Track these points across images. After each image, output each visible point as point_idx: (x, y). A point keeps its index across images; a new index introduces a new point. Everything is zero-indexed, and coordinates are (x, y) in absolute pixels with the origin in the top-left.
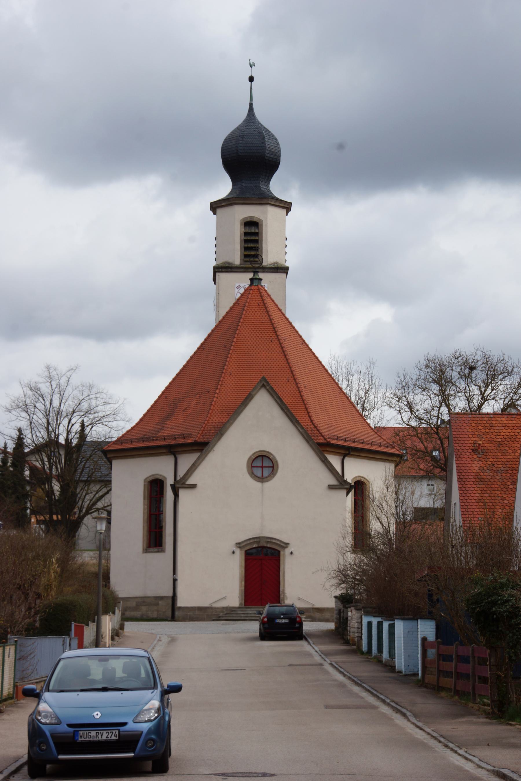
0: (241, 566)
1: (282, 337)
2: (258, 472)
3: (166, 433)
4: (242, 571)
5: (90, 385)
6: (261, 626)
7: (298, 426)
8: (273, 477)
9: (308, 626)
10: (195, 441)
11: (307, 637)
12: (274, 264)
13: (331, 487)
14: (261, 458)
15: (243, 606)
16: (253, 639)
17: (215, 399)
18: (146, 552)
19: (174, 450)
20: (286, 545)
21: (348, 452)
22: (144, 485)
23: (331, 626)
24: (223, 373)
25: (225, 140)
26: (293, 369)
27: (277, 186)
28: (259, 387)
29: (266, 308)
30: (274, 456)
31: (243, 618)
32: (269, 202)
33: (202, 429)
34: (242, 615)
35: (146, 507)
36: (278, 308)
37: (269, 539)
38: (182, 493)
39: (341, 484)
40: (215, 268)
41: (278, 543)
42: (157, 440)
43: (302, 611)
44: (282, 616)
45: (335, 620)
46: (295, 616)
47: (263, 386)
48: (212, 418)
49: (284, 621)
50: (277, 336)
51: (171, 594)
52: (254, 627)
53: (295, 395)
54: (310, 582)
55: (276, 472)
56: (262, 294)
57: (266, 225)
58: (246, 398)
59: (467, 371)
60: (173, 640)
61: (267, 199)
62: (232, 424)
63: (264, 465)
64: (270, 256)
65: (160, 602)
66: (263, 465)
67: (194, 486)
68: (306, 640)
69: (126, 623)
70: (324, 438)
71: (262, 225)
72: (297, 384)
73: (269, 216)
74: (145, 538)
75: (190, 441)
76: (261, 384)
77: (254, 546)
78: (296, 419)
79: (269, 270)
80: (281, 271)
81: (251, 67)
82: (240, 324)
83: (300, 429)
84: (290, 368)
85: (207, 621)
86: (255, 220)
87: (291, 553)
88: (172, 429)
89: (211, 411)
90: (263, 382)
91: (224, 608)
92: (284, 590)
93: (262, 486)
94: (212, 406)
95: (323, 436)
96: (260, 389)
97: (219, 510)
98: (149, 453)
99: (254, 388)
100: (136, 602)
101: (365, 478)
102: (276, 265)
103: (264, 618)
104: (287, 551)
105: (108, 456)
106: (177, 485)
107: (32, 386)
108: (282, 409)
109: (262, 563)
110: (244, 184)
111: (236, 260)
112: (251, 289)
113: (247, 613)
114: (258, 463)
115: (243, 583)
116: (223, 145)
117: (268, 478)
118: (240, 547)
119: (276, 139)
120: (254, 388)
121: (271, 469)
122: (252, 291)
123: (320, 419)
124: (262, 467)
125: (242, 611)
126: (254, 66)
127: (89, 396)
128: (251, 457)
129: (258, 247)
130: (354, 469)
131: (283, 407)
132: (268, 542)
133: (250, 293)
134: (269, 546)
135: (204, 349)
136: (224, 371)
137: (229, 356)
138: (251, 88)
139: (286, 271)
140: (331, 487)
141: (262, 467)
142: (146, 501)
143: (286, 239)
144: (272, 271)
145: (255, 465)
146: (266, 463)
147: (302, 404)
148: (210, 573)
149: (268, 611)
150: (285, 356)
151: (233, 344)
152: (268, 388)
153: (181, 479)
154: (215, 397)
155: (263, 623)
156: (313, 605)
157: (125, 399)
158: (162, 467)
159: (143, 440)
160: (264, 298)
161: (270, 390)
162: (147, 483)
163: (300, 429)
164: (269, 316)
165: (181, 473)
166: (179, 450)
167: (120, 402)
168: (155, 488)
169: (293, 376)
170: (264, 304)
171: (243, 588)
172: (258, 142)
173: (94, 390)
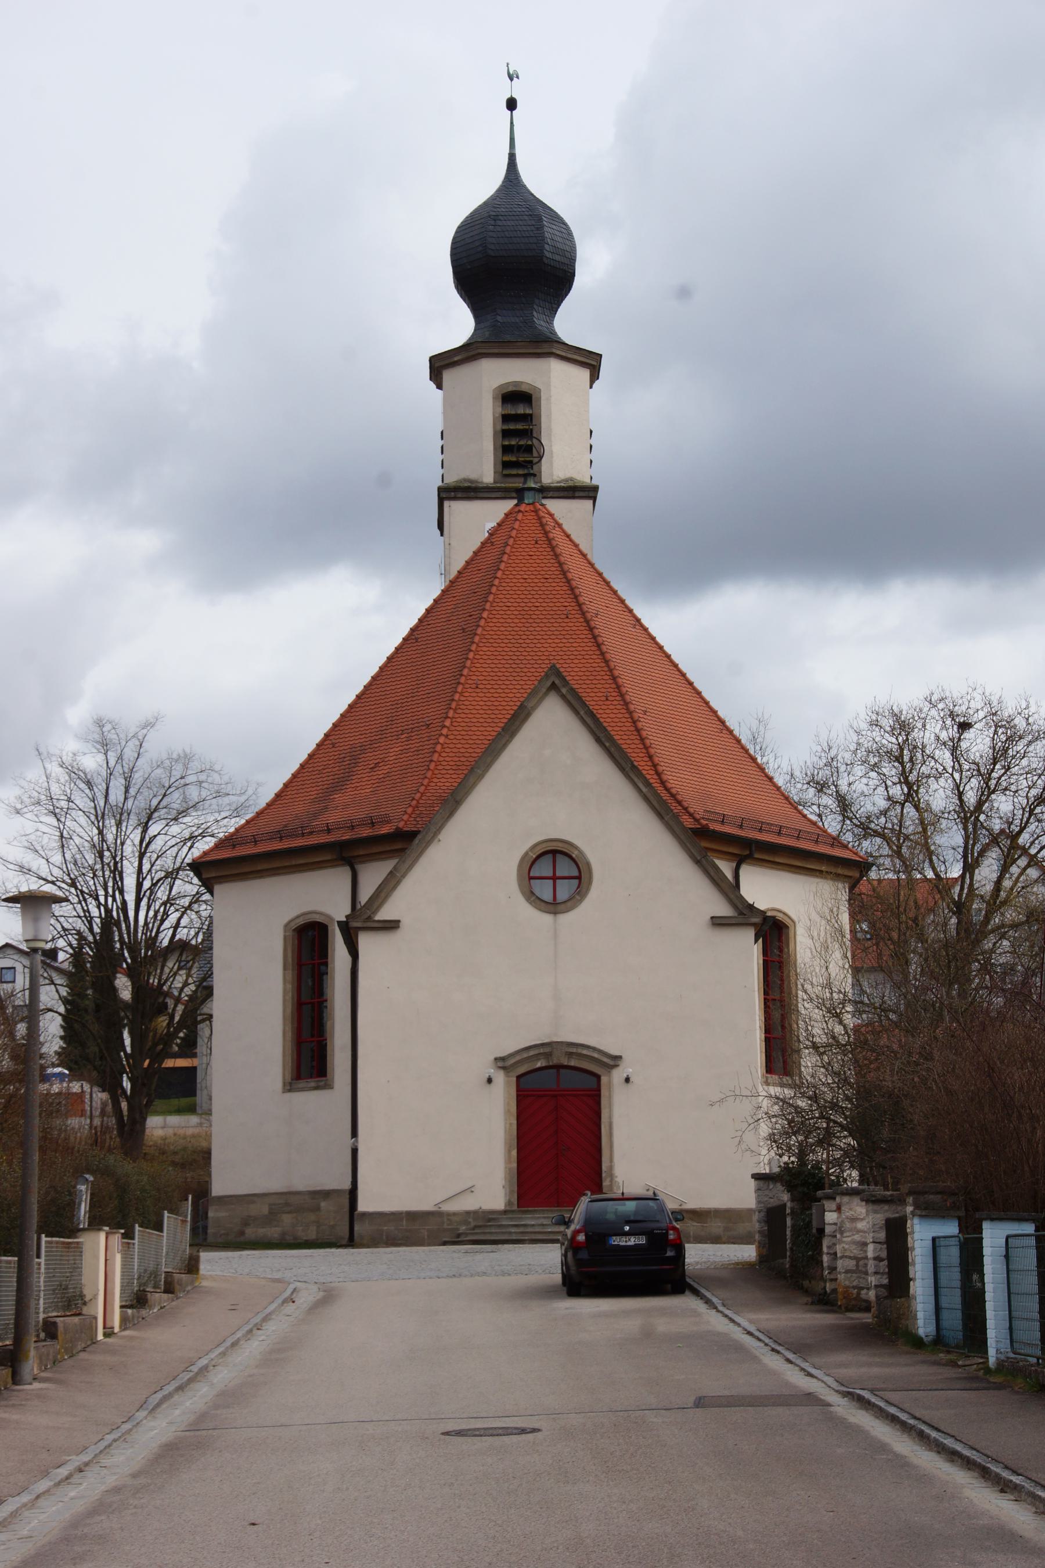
0: (507, 1112)
1: (590, 608)
2: (545, 890)
3: (332, 817)
4: (511, 1124)
5: (186, 756)
6: (570, 1255)
7: (636, 780)
8: (581, 901)
9: (697, 1256)
10: (398, 828)
11: (696, 1286)
12: (566, 480)
13: (718, 922)
14: (550, 856)
15: (515, 1207)
16: (547, 1293)
17: (442, 740)
18: (290, 1091)
19: (346, 853)
20: (616, 1060)
21: (747, 852)
22: (285, 938)
23: (748, 1252)
24: (459, 683)
25: (459, 227)
26: (616, 673)
27: (569, 322)
28: (544, 690)
29: (553, 548)
30: (581, 852)
31: (514, 1237)
32: (554, 351)
33: (414, 803)
34: (513, 1230)
35: (289, 986)
36: (580, 551)
37: (573, 1049)
38: (366, 942)
39: (744, 915)
40: (439, 489)
41: (596, 1055)
42: (311, 833)
43: (680, 1215)
44: (627, 1228)
45: (757, 1237)
46: (663, 1225)
47: (553, 687)
48: (435, 780)
49: (632, 1241)
50: (580, 605)
51: (347, 1185)
52: (547, 1261)
53: (624, 729)
54: (696, 1135)
55: (588, 889)
56: (544, 520)
57: (549, 399)
58: (513, 715)
59: (953, 732)
60: (328, 1297)
61: (545, 345)
62: (481, 777)
63: (558, 874)
64: (559, 463)
65: (323, 1204)
66: (556, 873)
67: (392, 926)
68: (696, 1293)
69: (205, 1256)
70: (694, 818)
71: (540, 398)
72: (626, 704)
73: (555, 382)
74: (289, 1059)
75: (385, 830)
76: (549, 684)
77: (539, 1065)
78: (632, 762)
79: (556, 494)
80: (581, 494)
81: (511, 79)
82: (496, 582)
83: (641, 785)
84: (611, 671)
85: (429, 1245)
86: (524, 388)
87: (627, 1080)
88: (347, 810)
89: (432, 766)
90: (553, 678)
91: (468, 1213)
92: (611, 1168)
93: (555, 921)
94: (436, 755)
95: (691, 815)
96: (546, 694)
97: (454, 983)
98: (294, 863)
99: (533, 693)
100: (270, 1205)
101: (784, 914)
102: (571, 484)
103: (576, 1232)
104: (617, 1076)
105: (204, 876)
106: (354, 924)
107: (64, 758)
108: (598, 740)
109: (558, 1107)
110: (499, 318)
111: (487, 473)
112: (520, 511)
113: (525, 1226)
114: (544, 868)
115: (514, 1153)
116: (454, 238)
117: (569, 904)
118: (504, 1068)
119: (565, 224)
120: (533, 693)
121: (576, 881)
122: (520, 514)
123: (681, 780)
124: (554, 878)
125: (511, 1219)
126: (518, 77)
127: (182, 778)
128: (526, 854)
129: (532, 430)
130: (764, 889)
131: (601, 735)
132: (570, 1055)
133: (516, 520)
134: (572, 1063)
135: (416, 639)
136: (462, 680)
137: (474, 647)
138: (512, 123)
139: (591, 494)
140: (718, 922)
141: (554, 878)
142: (290, 973)
143: (591, 432)
144: (562, 494)
145: (538, 875)
146: (564, 868)
147: (641, 746)
148: (435, 1131)
149: (587, 1211)
150: (599, 646)
151: (482, 623)
152: (564, 691)
153: (362, 907)
154: (442, 734)
155: (573, 1246)
156: (682, 1203)
157: (259, 784)
158: (326, 894)
159: (280, 835)
160: (548, 528)
161: (569, 697)
162: (290, 933)
163: (641, 785)
164: (561, 564)
165: (365, 895)
166: (361, 853)
167: (250, 792)
168: (309, 948)
169: (618, 687)
170: (549, 541)
171: (515, 1165)
172: (529, 228)
173: (195, 766)
